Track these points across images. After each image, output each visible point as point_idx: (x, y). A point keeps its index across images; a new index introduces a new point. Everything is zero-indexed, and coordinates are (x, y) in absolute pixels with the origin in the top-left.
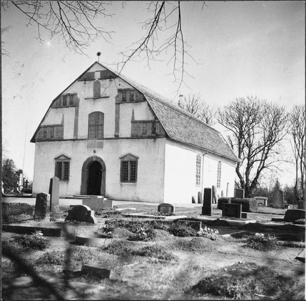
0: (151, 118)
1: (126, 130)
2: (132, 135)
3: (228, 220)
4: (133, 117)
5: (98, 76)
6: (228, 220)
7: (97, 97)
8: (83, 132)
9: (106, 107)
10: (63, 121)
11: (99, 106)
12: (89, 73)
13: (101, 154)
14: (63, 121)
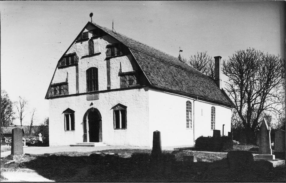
4: (121, 69)
9: (99, 62)
10: (67, 80)
11: (93, 62)
14: (67, 80)
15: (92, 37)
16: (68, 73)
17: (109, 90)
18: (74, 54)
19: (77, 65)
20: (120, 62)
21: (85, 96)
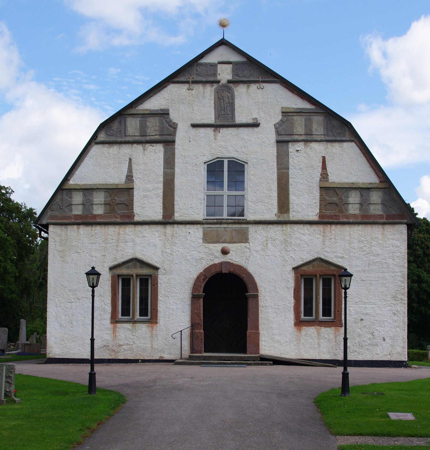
0: (369, 178)
1: (306, 202)
2: (321, 216)
3: (194, 355)
4: (324, 175)
5: (225, 74)
6: (194, 355)
7: (225, 119)
8: (192, 201)
9: (256, 149)
10: (130, 177)
11: (228, 144)
12: (206, 65)
13: (238, 255)
14: (130, 177)
15: (230, 77)
16: (134, 160)
17: (168, 220)
18: (164, 114)
19: (168, 143)
20: (324, 158)
21: (197, 232)
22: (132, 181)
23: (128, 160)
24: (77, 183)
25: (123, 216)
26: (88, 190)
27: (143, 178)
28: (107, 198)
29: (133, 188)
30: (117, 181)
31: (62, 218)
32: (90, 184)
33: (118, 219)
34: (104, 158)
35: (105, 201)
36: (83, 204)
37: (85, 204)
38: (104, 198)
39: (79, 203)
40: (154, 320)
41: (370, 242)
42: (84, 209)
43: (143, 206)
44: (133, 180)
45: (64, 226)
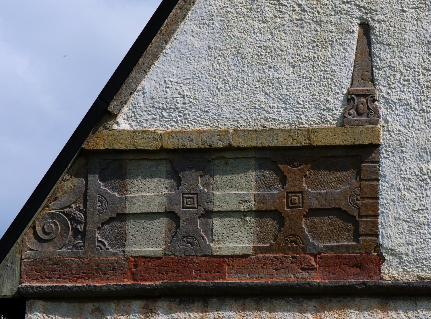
10: (361, 102)
14: (361, 102)
22: (373, 116)
23: (357, 29)
24: (146, 126)
25: (334, 261)
26: (190, 159)
27: (419, 102)
28: (269, 187)
29: (378, 146)
30: (309, 119)
31: (86, 272)
32: (200, 132)
33: (313, 273)
34: (257, 25)
35: (259, 199)
36: (171, 215)
37: (179, 210)
38: (258, 188)
39: (153, 208)
40: (376, 186)
41: (254, 102)
42: (173, 234)
43: (420, 218)
44: (376, 111)
45: (90, 306)
